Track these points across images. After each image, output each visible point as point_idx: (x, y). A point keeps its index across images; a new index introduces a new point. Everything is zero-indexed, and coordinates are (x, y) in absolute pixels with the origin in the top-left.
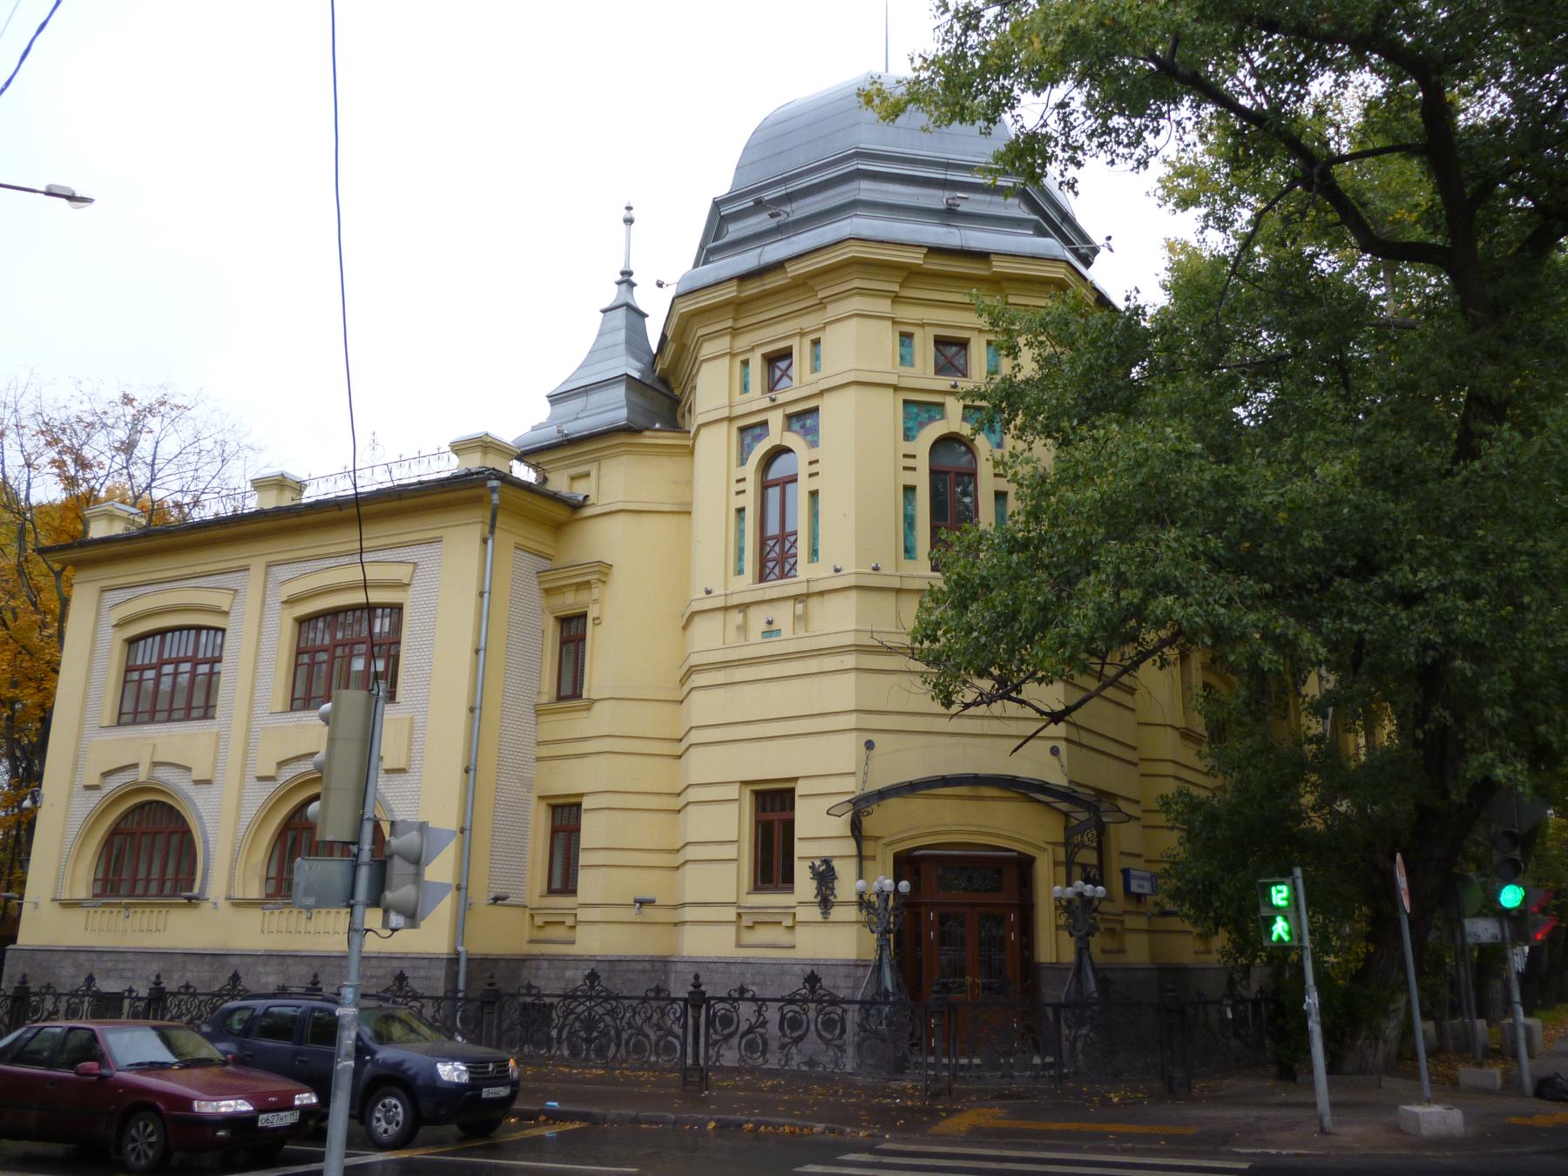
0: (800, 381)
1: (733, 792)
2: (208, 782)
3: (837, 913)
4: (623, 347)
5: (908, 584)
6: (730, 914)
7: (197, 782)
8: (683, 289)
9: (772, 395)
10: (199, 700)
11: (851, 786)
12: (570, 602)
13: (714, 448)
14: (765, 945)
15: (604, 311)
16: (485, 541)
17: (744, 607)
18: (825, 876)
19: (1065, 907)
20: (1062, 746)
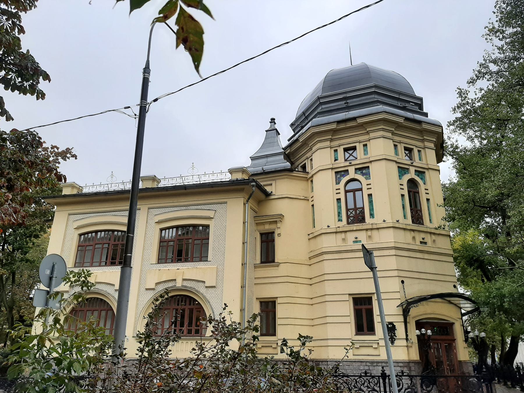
1: (347, 297)
2: (214, 287)
3: (397, 343)
5: (338, 230)
7: (207, 287)
12: (267, 228)
14: (366, 354)
15: (266, 131)
18: (391, 329)
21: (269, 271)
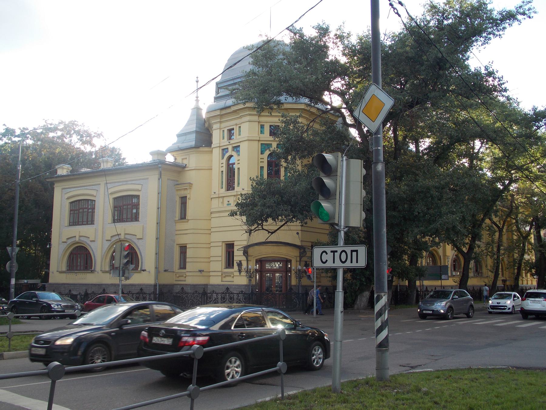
0: (236, 138)
1: (220, 244)
2: (94, 241)
6: (220, 274)
10: (90, 219)
11: (245, 243)
12: (183, 193)
16: (159, 179)
18: (240, 264)
20: (300, 232)
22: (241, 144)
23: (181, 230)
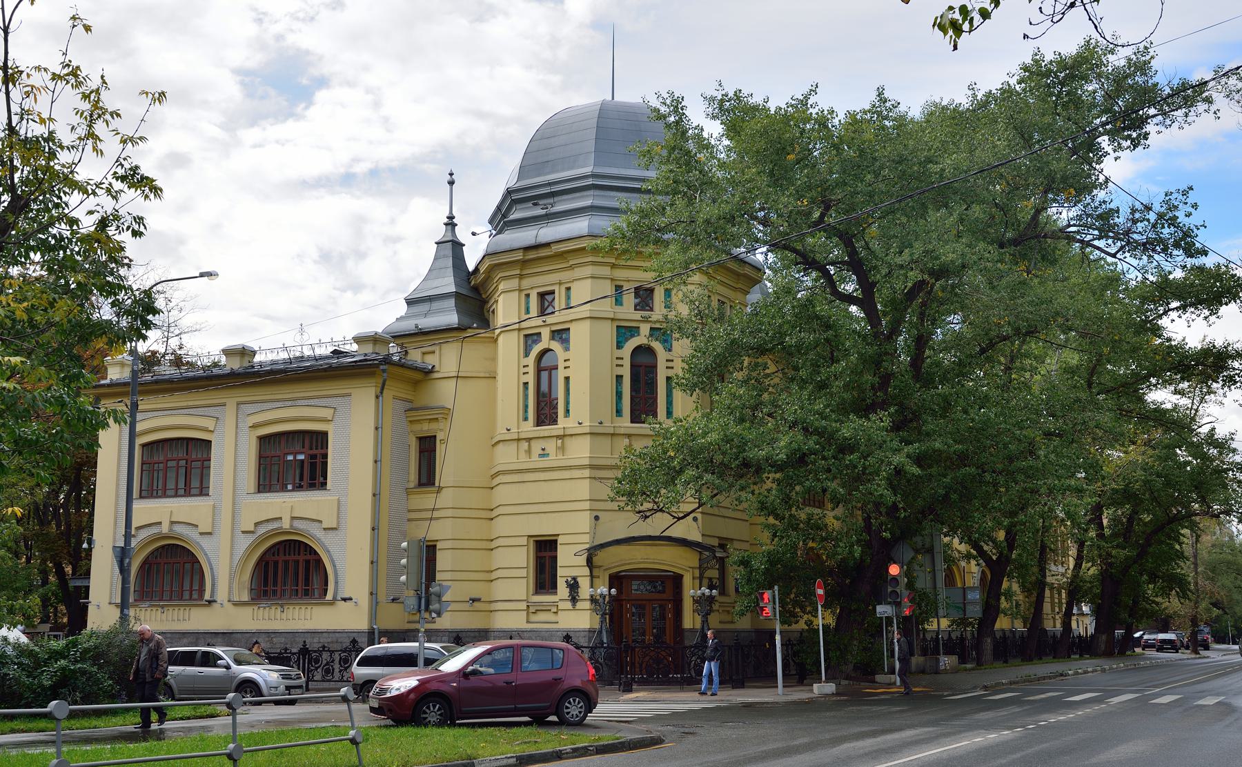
1: (524, 541)
2: (210, 534)
3: (579, 605)
4: (451, 270)
6: (523, 606)
7: (201, 534)
8: (490, 251)
9: (544, 318)
12: (426, 429)
13: (508, 346)
14: (542, 621)
16: (377, 397)
17: (529, 440)
18: (573, 586)
19: (697, 601)
21: (425, 500)
22: (573, 327)
23: (420, 510)
